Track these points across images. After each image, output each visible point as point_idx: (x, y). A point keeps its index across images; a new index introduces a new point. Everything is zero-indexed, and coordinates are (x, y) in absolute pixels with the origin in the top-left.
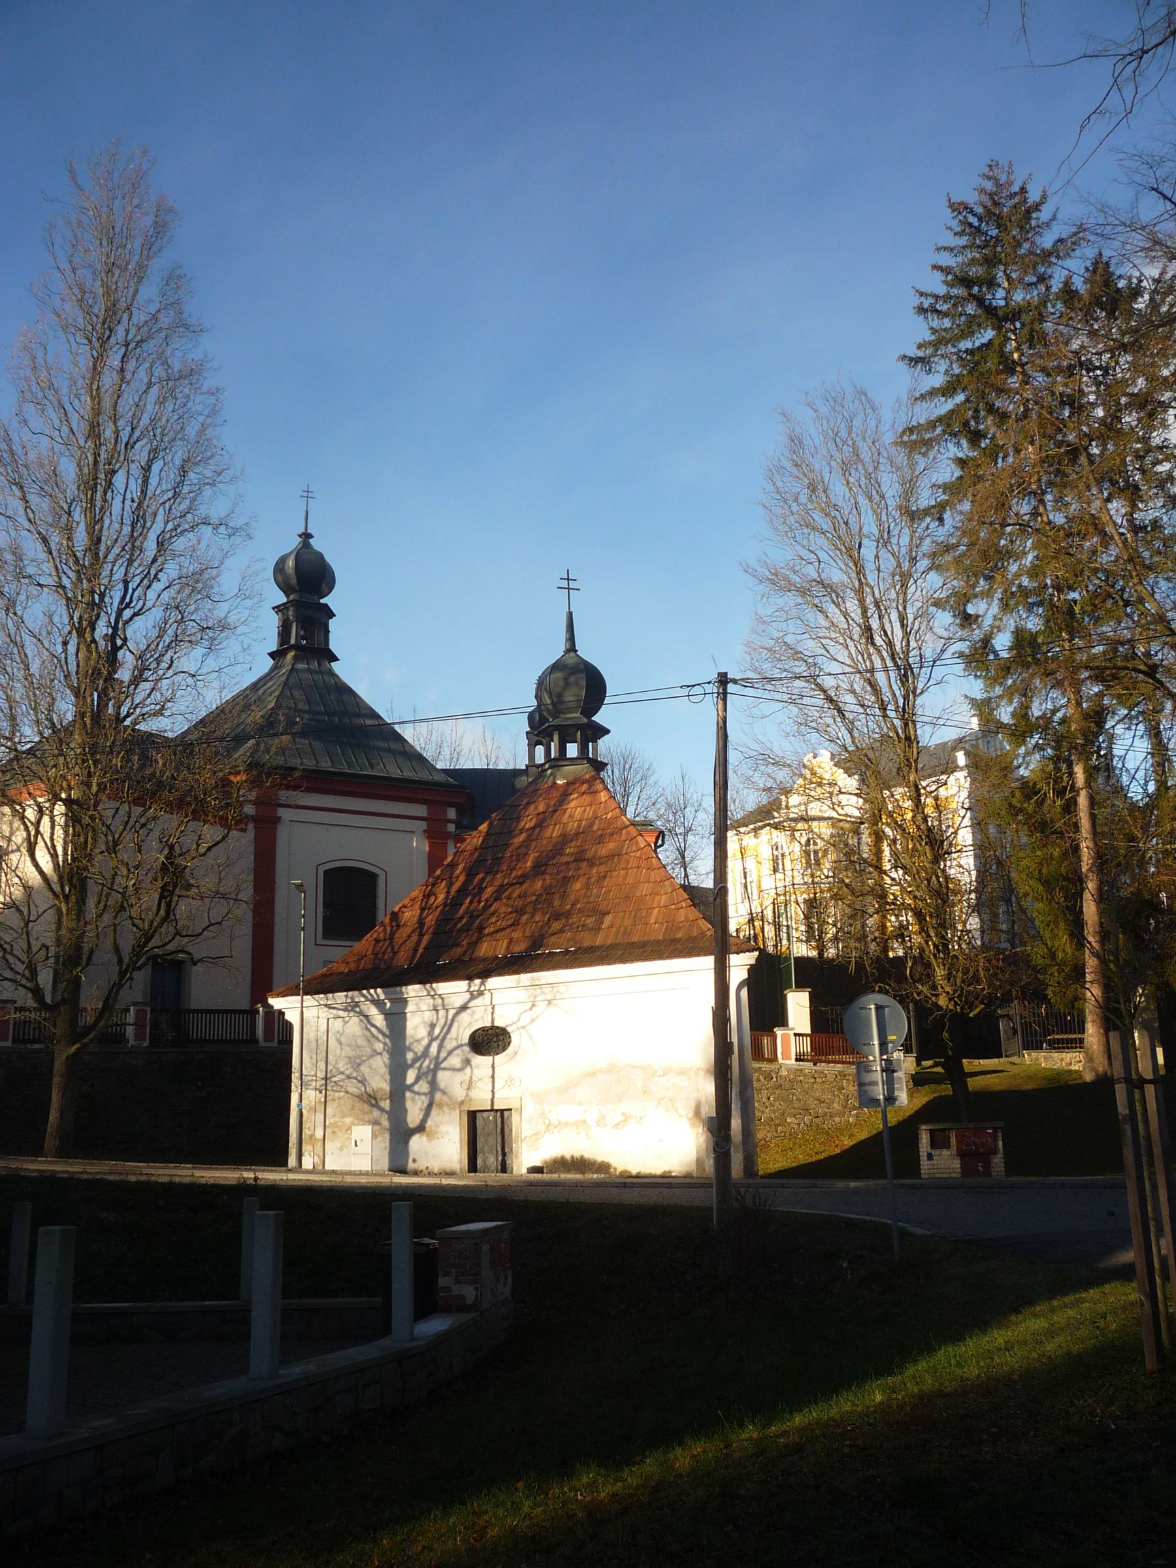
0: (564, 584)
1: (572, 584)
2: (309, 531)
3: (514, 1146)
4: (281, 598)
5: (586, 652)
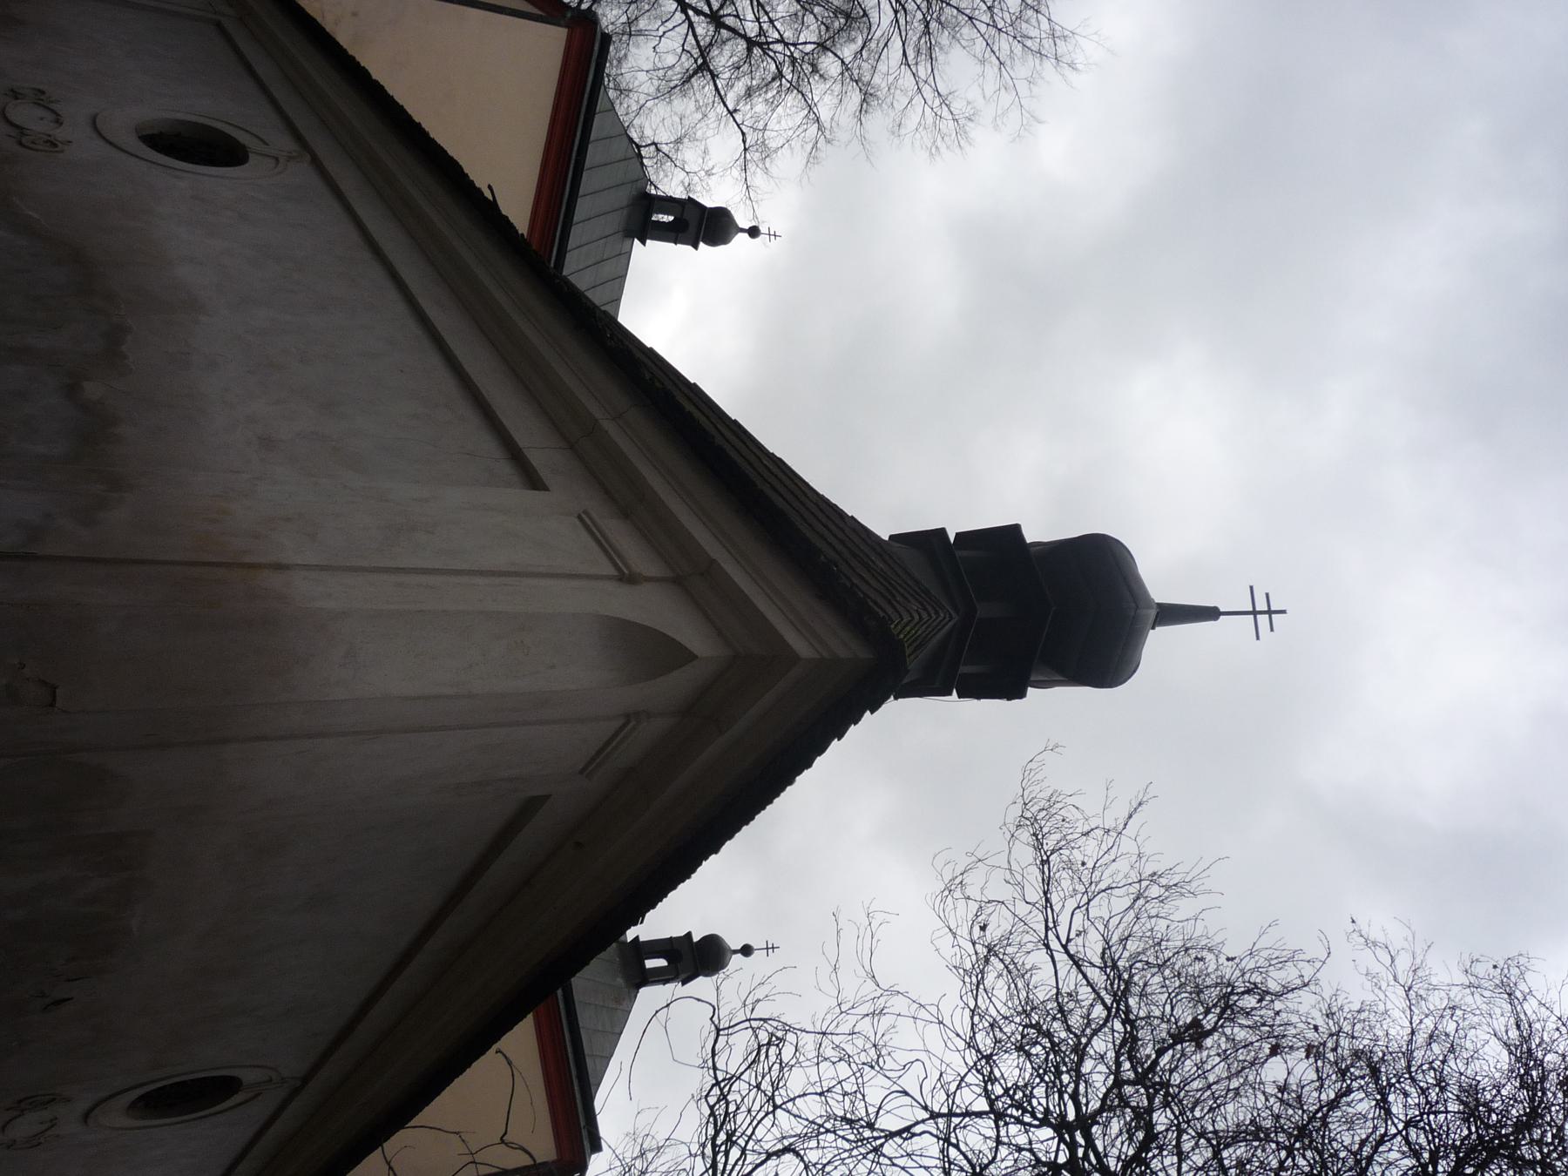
0: (770, 946)
1: (770, 951)
5: (1159, 643)
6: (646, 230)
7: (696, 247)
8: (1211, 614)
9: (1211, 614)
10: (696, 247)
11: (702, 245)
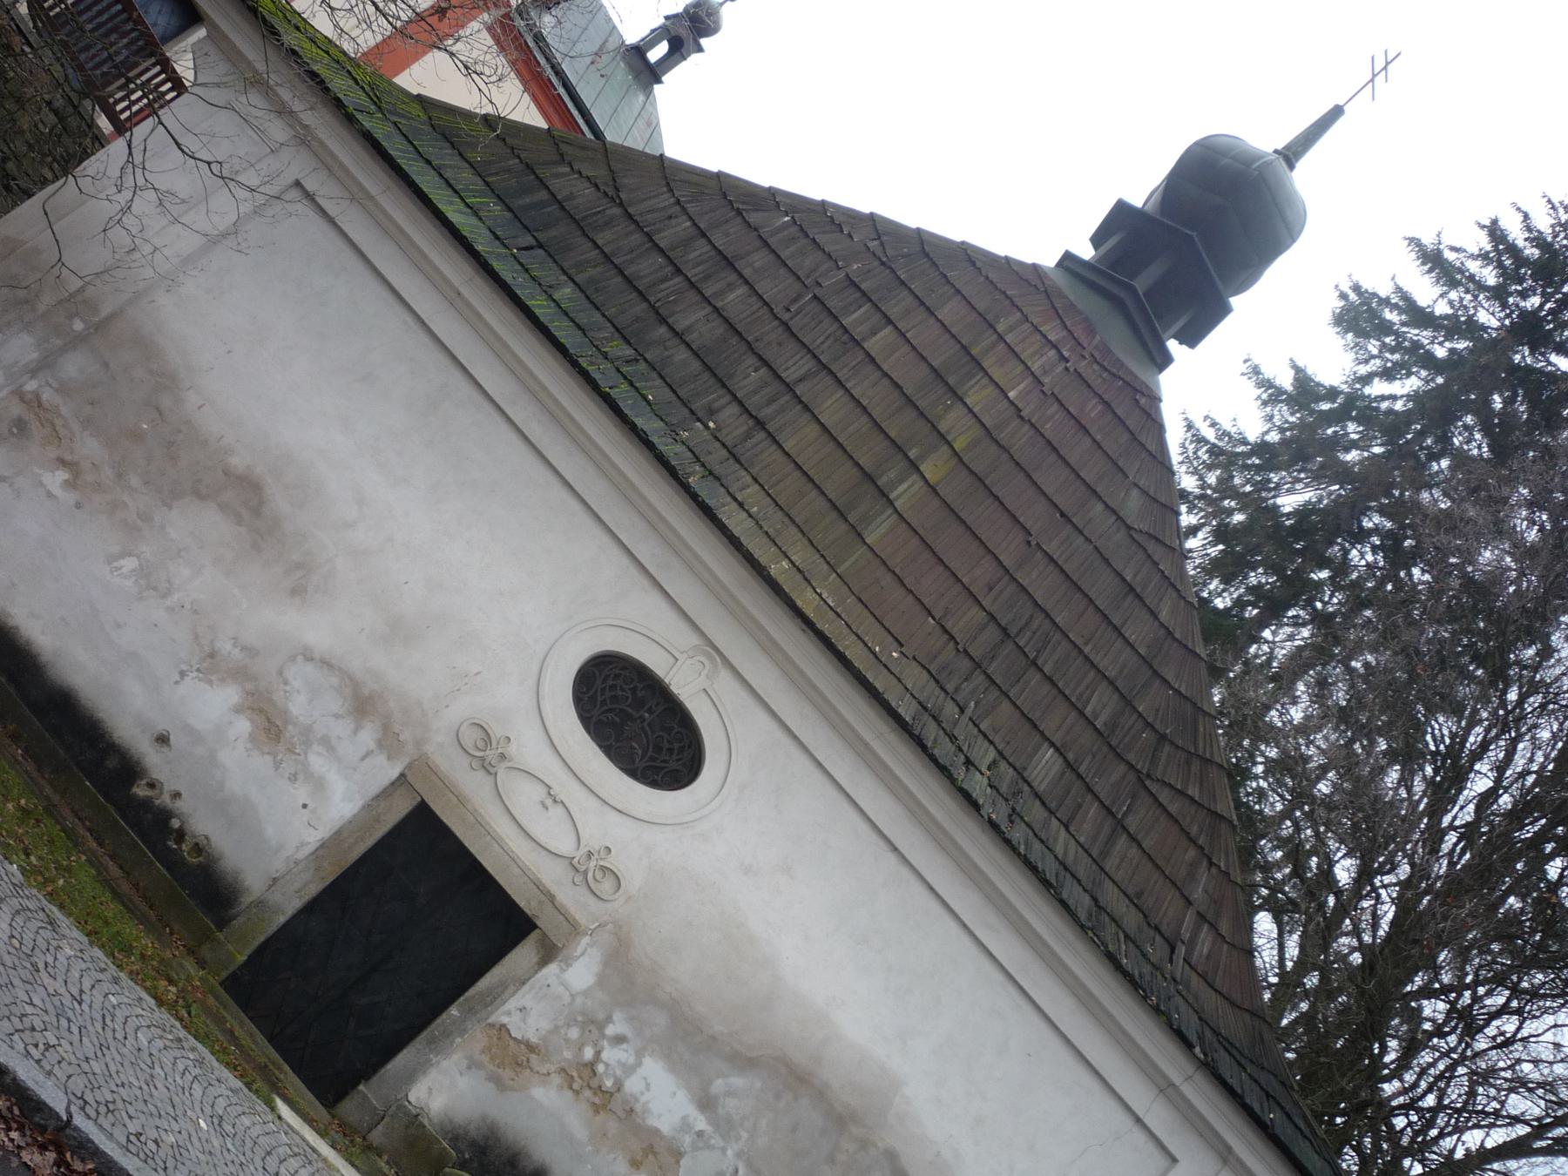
2: (1345, 108)
3: (454, 1011)
4: (1087, 252)
6: (651, 75)
7: (700, 49)
8: (1336, 112)
9: (1336, 112)
10: (700, 49)
11: (704, 42)
